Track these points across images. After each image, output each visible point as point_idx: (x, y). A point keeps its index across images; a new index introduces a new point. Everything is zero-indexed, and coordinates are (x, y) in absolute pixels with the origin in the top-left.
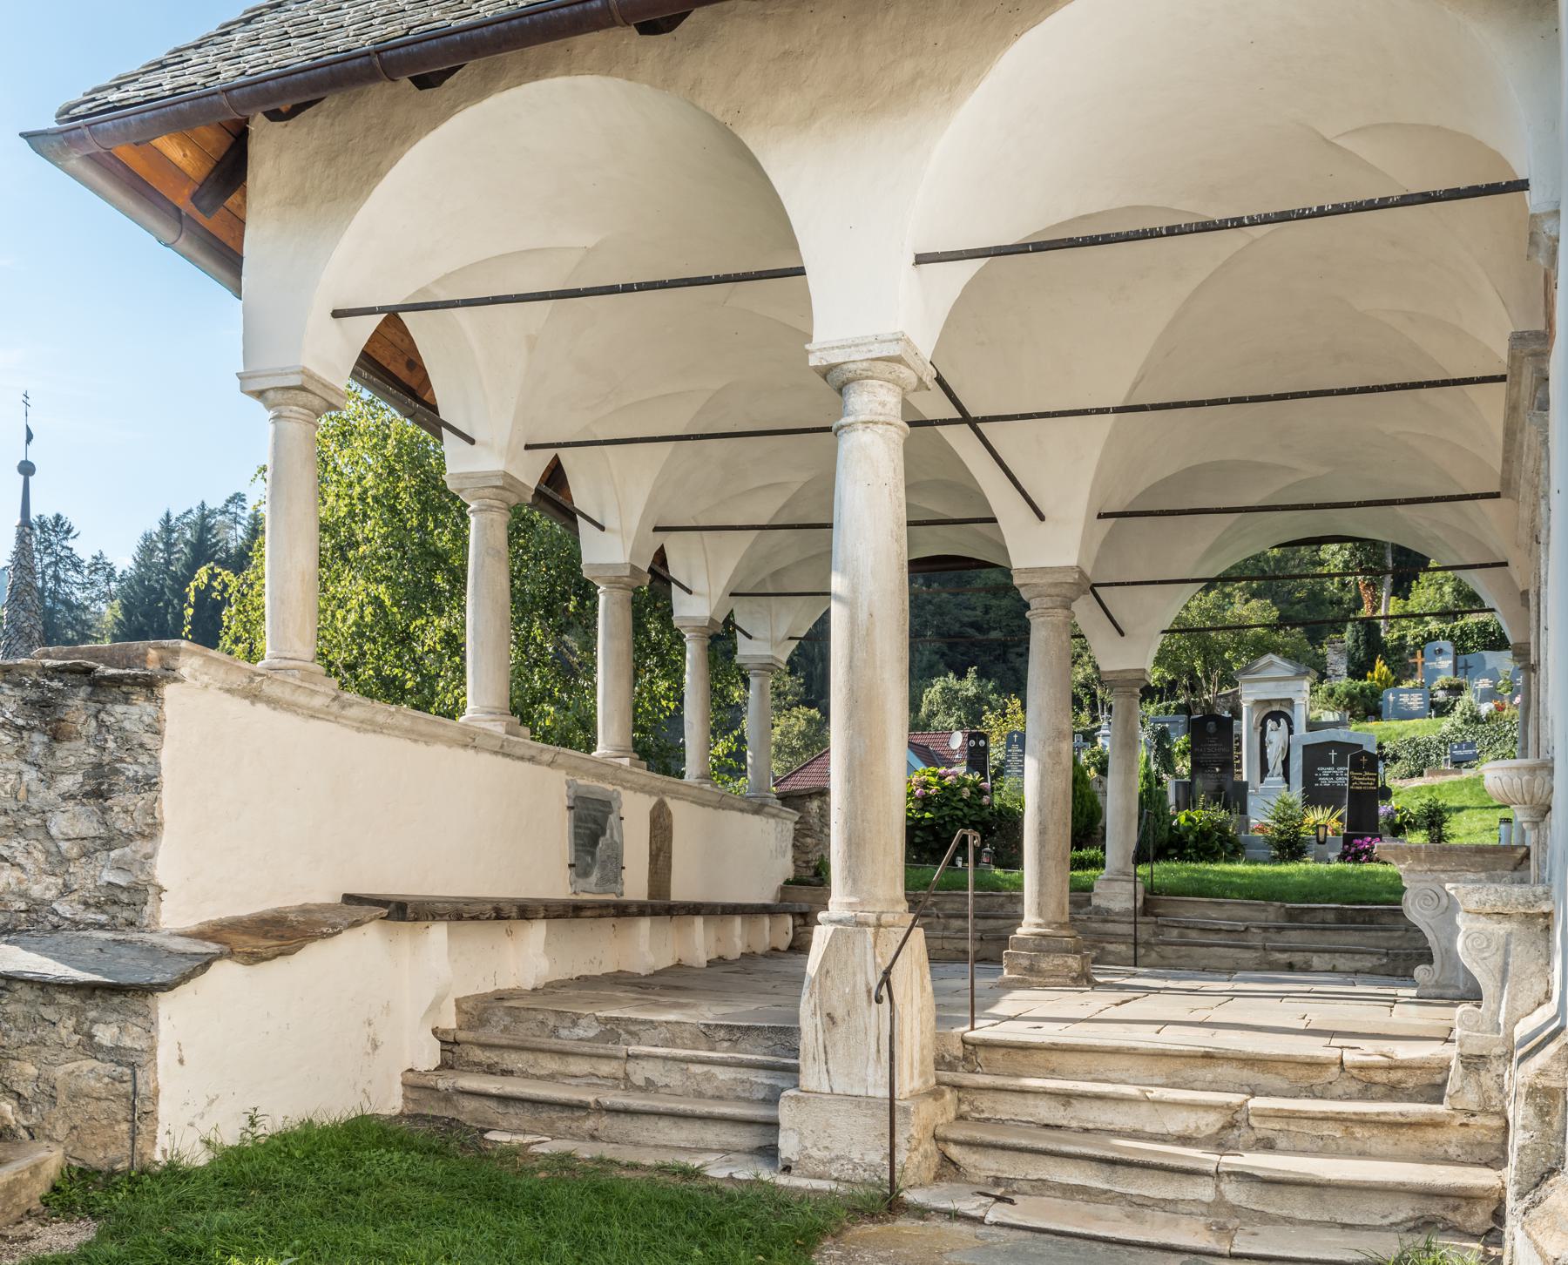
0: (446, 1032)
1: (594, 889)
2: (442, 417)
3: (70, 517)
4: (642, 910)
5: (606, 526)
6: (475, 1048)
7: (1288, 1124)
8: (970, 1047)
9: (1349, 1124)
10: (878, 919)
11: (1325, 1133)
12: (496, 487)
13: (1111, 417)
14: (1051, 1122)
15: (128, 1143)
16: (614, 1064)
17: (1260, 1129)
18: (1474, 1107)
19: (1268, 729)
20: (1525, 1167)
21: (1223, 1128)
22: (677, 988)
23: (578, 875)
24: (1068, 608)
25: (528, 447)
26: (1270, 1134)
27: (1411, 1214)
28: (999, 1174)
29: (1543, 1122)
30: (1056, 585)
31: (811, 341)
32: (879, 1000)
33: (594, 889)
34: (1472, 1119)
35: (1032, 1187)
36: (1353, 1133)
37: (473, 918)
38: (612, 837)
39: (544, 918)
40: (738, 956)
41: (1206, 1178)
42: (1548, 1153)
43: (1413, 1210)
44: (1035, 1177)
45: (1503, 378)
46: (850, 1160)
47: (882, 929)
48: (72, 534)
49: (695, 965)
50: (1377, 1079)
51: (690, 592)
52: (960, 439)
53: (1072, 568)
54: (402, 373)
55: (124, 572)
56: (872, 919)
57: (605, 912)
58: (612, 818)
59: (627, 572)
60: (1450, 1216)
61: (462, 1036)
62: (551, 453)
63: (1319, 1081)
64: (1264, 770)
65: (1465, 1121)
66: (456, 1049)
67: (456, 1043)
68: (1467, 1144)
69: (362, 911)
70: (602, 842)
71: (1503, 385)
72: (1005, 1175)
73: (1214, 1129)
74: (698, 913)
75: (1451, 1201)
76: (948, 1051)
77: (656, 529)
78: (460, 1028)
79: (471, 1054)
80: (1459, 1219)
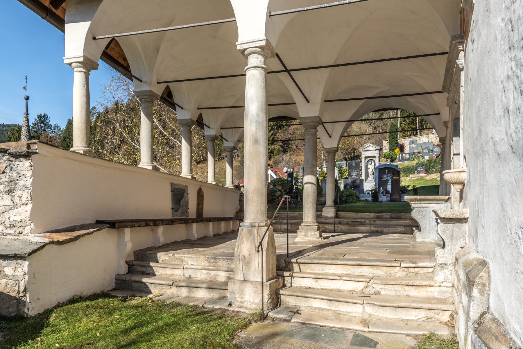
0: (130, 261)
1: (180, 215)
2: (204, 123)
3: (48, 114)
4: (194, 221)
5: (143, 80)
6: (139, 266)
7: (385, 286)
8: (287, 263)
9: (404, 286)
10: (259, 225)
11: (396, 289)
12: (149, 95)
13: (329, 69)
14: (312, 287)
15: (16, 307)
16: (180, 270)
17: (376, 288)
18: (443, 280)
19: (369, 164)
20: (474, 311)
21: (364, 288)
22: (203, 244)
23: (175, 211)
24: (316, 129)
25: (158, 83)
26: (378, 289)
27: (424, 316)
28: (296, 305)
29: (481, 295)
30: (312, 122)
31: (238, 42)
32: (258, 251)
33: (180, 215)
34: (442, 284)
35: (306, 308)
36: (404, 289)
37: (138, 226)
38: (185, 199)
39: (162, 225)
40: (223, 233)
41: (360, 305)
42: (483, 306)
43: (425, 314)
44: (307, 305)
45: (447, 53)
46: (250, 301)
47: (260, 228)
48: (48, 118)
49: (210, 236)
50: (411, 271)
51: (209, 128)
52: (284, 77)
53: (317, 117)
54: (122, 62)
55: (63, 129)
56: (257, 225)
57: (181, 222)
58: (185, 194)
59: (190, 121)
60: (436, 316)
61: (135, 263)
62: (166, 84)
63: (393, 272)
64: (367, 176)
65: (440, 285)
66: (133, 267)
67: (133, 265)
68: (440, 292)
69: (101, 225)
70: (182, 200)
71: (447, 55)
72: (297, 305)
73: (361, 288)
74: (210, 221)
75: (437, 311)
76: (280, 265)
77: (198, 109)
78: (135, 260)
79: (137, 268)
80: (439, 317)
